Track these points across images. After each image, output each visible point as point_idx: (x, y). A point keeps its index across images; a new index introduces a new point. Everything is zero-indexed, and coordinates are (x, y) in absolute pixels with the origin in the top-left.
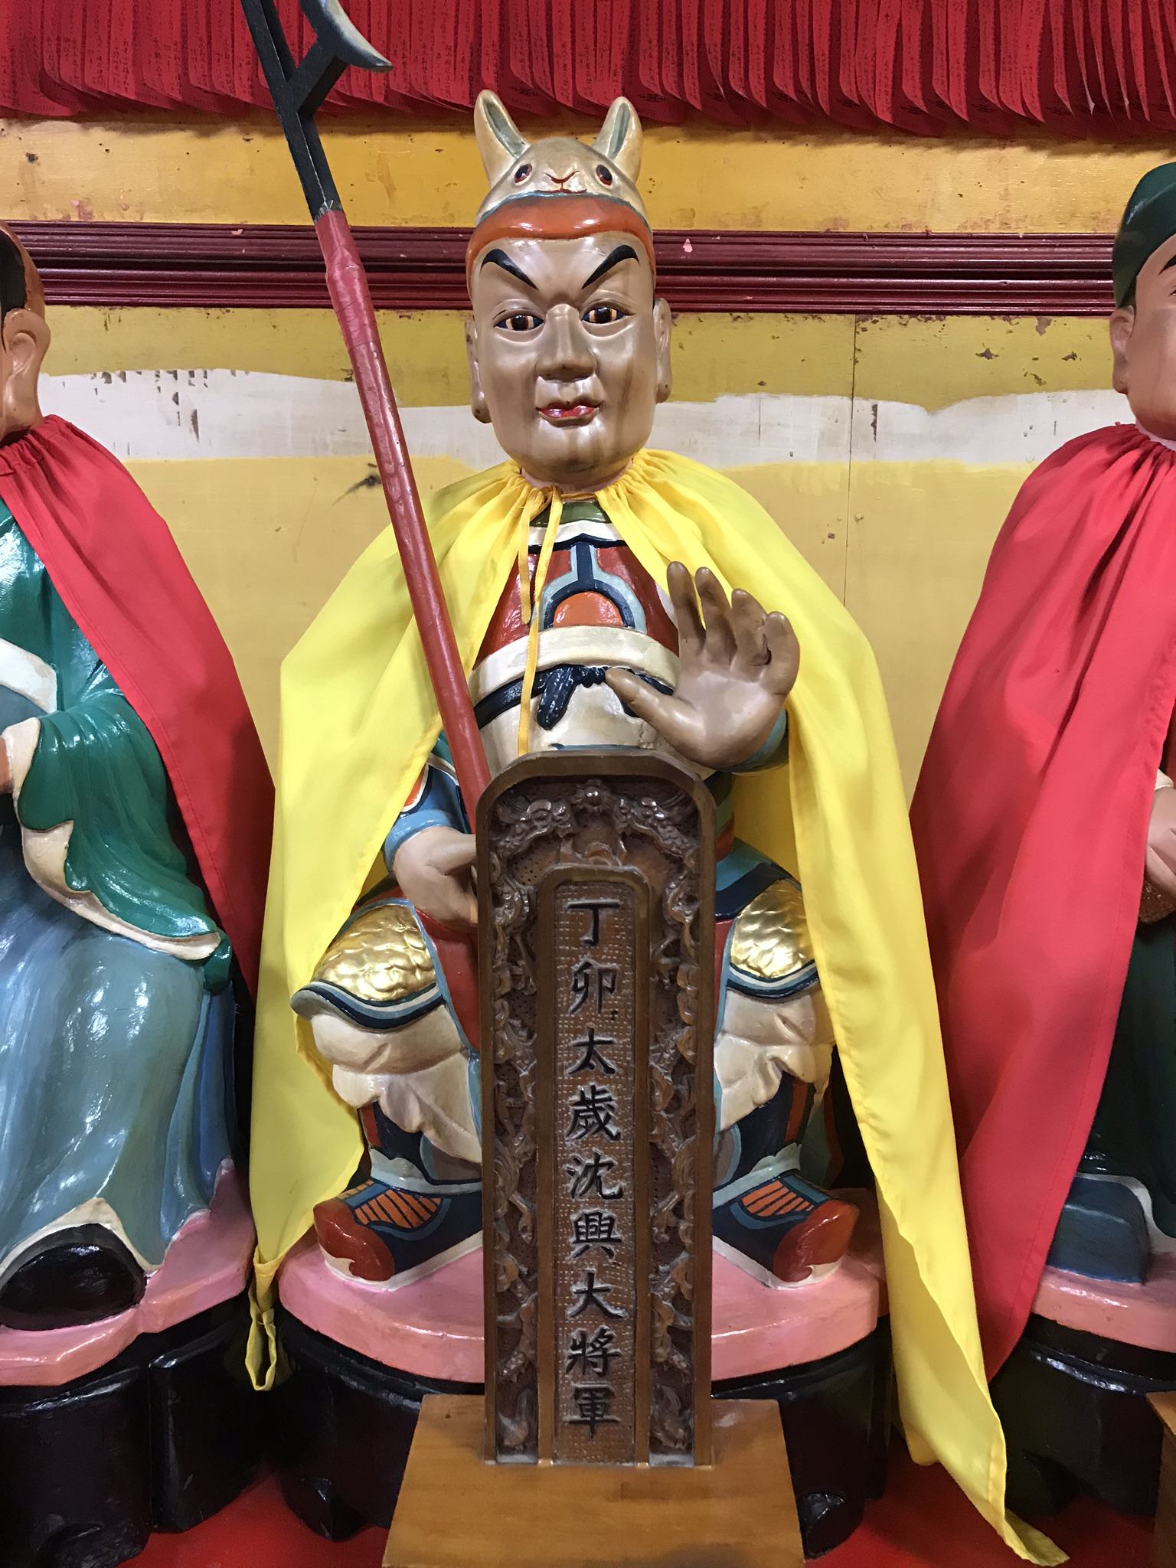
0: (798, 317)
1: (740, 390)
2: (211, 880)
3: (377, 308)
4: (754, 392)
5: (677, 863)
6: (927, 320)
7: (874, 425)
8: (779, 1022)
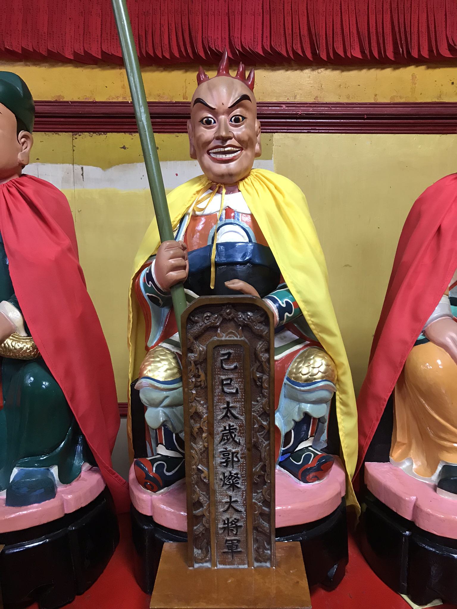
0: (50, 134)
3: (154, 132)
6: (100, 134)
7: (82, 175)
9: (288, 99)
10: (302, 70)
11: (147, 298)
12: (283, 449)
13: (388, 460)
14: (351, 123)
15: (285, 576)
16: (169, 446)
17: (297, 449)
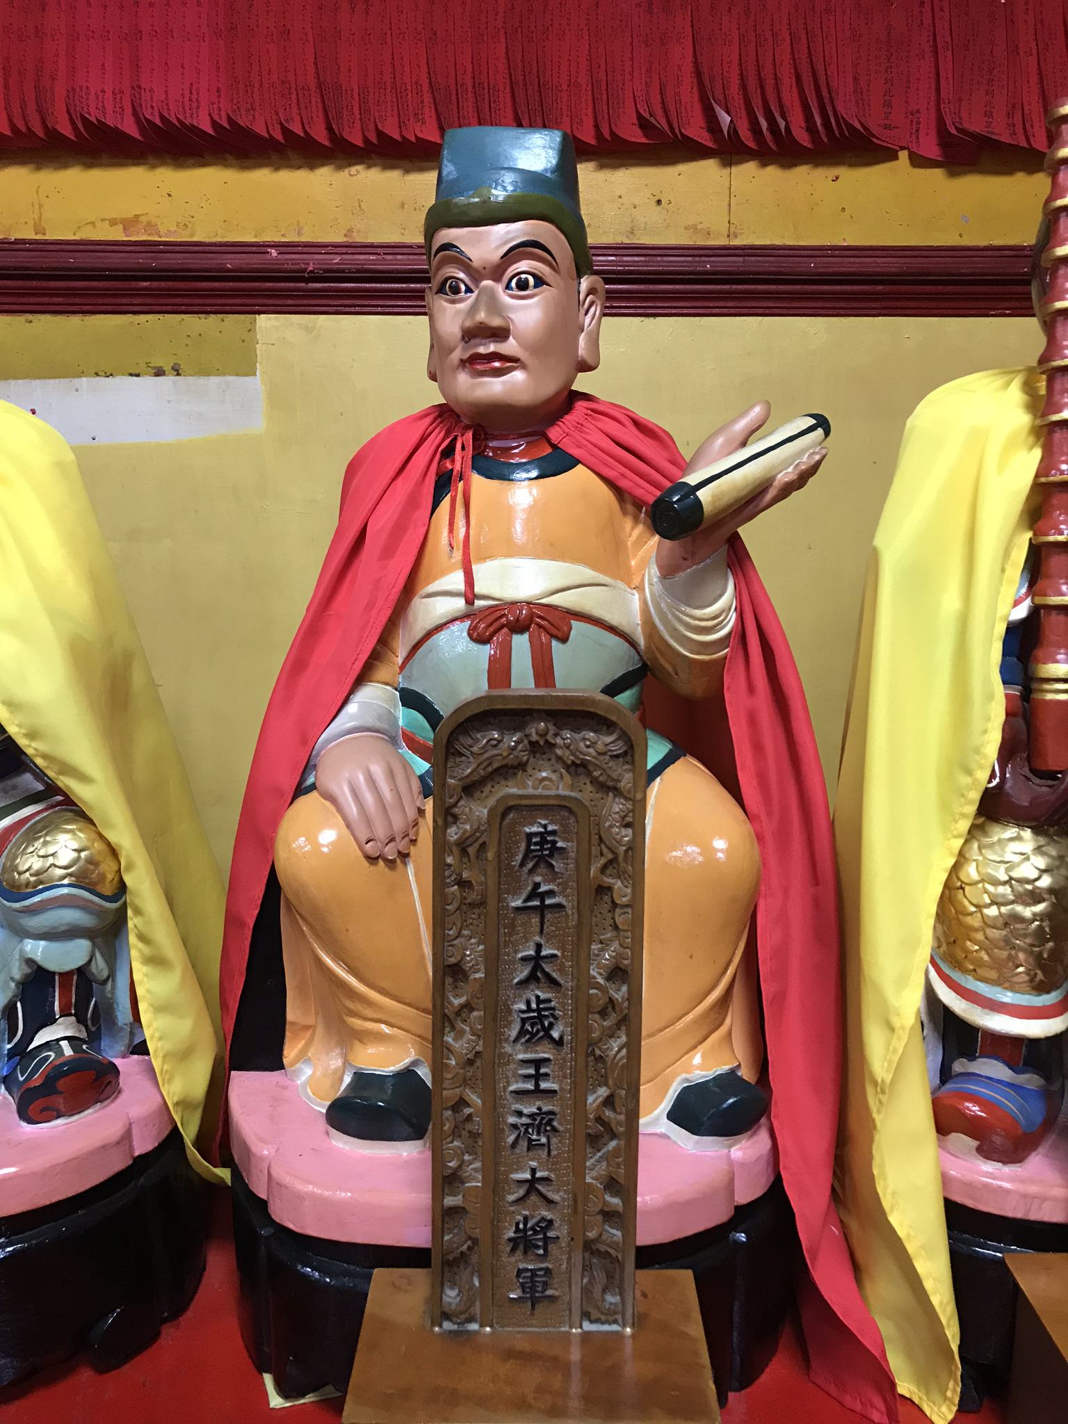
2: (505, 822)
9: (283, 235)
10: (312, 167)
12: (9, 1046)
13: (281, 1067)
14: (330, 290)
17: (31, 1047)
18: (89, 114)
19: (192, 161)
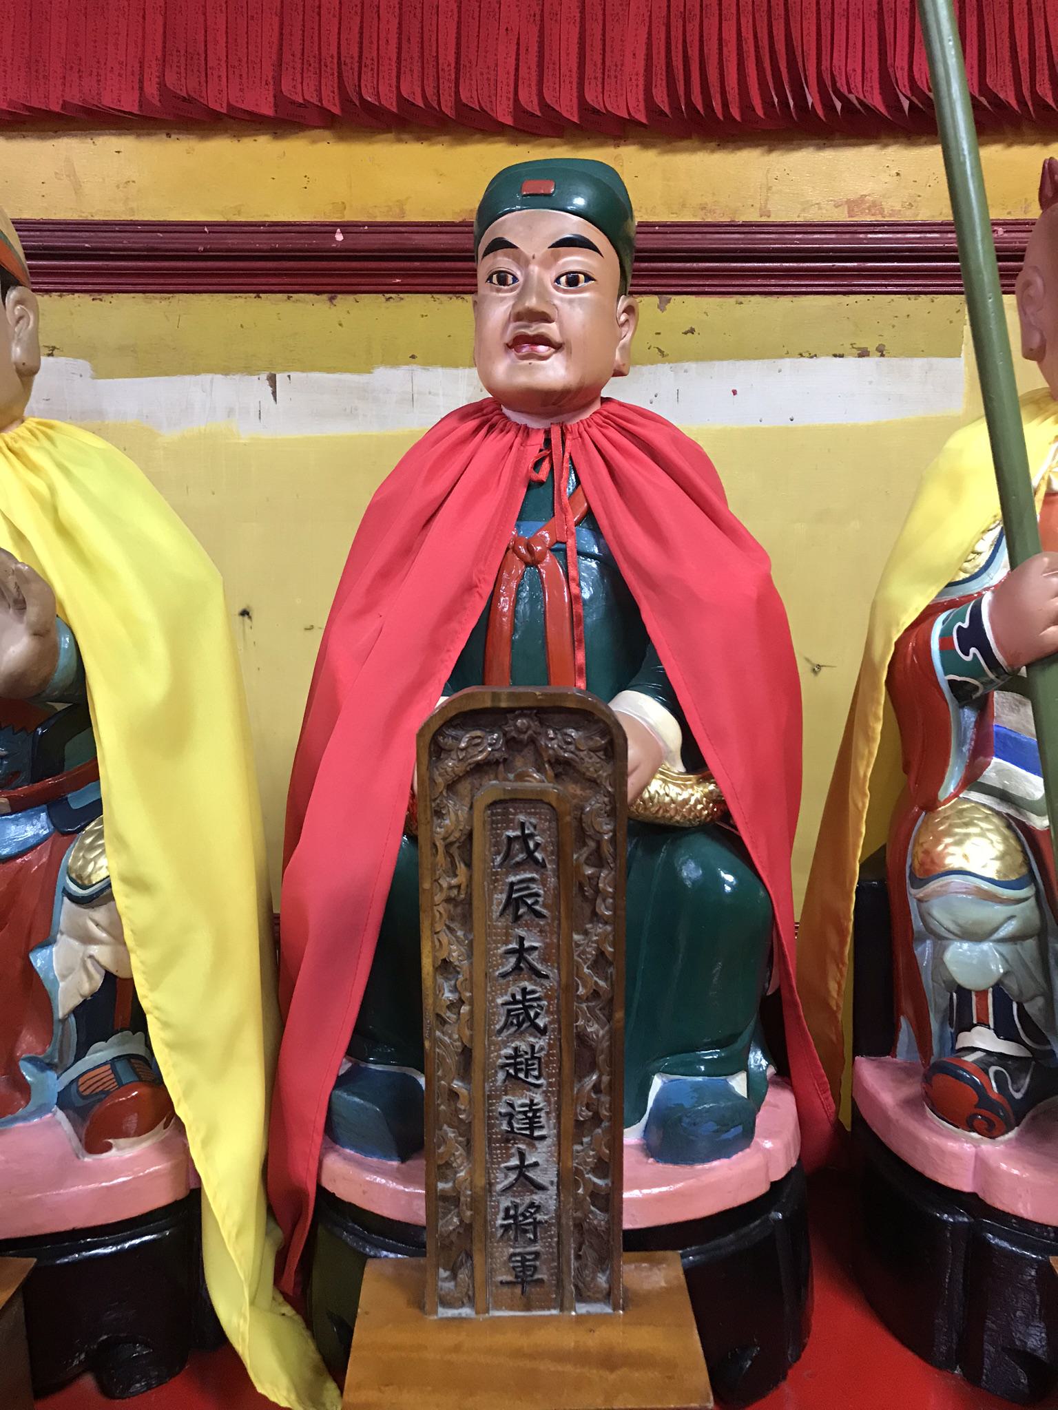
1: (394, 363)
3: (1005, 293)
4: (407, 364)
5: (594, 783)
8: (92, 925)
9: (1009, 213)
11: (945, 687)
15: (657, 1335)
16: (1004, 1030)
18: (850, 92)
19: (924, 139)
